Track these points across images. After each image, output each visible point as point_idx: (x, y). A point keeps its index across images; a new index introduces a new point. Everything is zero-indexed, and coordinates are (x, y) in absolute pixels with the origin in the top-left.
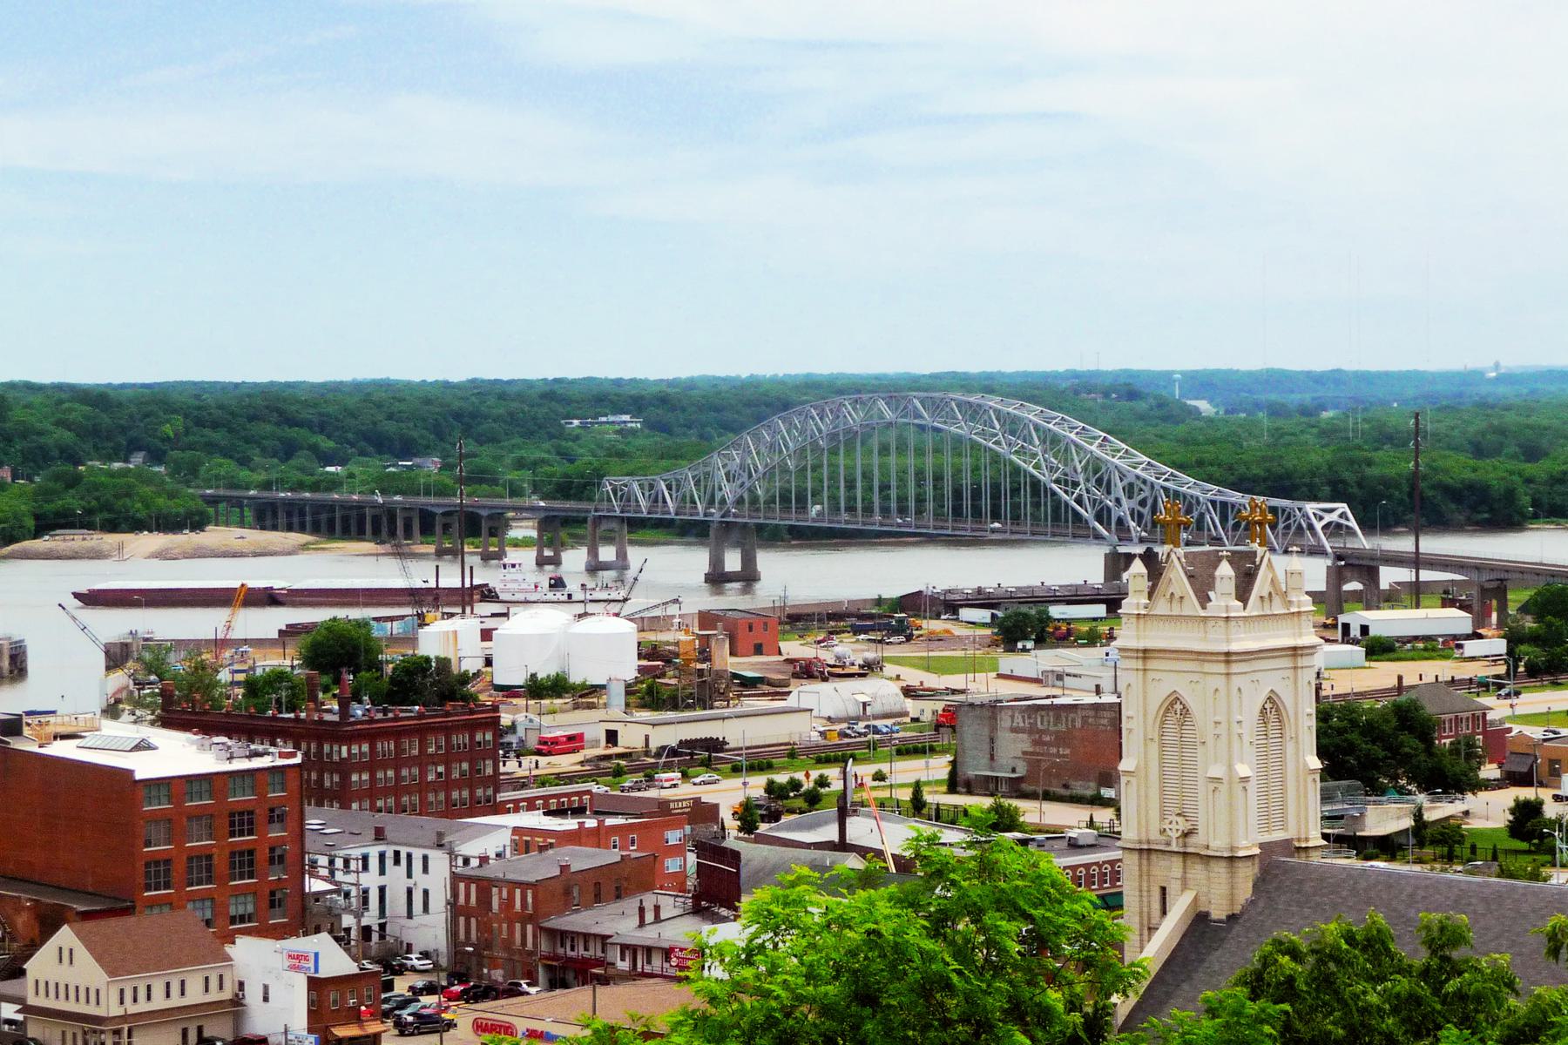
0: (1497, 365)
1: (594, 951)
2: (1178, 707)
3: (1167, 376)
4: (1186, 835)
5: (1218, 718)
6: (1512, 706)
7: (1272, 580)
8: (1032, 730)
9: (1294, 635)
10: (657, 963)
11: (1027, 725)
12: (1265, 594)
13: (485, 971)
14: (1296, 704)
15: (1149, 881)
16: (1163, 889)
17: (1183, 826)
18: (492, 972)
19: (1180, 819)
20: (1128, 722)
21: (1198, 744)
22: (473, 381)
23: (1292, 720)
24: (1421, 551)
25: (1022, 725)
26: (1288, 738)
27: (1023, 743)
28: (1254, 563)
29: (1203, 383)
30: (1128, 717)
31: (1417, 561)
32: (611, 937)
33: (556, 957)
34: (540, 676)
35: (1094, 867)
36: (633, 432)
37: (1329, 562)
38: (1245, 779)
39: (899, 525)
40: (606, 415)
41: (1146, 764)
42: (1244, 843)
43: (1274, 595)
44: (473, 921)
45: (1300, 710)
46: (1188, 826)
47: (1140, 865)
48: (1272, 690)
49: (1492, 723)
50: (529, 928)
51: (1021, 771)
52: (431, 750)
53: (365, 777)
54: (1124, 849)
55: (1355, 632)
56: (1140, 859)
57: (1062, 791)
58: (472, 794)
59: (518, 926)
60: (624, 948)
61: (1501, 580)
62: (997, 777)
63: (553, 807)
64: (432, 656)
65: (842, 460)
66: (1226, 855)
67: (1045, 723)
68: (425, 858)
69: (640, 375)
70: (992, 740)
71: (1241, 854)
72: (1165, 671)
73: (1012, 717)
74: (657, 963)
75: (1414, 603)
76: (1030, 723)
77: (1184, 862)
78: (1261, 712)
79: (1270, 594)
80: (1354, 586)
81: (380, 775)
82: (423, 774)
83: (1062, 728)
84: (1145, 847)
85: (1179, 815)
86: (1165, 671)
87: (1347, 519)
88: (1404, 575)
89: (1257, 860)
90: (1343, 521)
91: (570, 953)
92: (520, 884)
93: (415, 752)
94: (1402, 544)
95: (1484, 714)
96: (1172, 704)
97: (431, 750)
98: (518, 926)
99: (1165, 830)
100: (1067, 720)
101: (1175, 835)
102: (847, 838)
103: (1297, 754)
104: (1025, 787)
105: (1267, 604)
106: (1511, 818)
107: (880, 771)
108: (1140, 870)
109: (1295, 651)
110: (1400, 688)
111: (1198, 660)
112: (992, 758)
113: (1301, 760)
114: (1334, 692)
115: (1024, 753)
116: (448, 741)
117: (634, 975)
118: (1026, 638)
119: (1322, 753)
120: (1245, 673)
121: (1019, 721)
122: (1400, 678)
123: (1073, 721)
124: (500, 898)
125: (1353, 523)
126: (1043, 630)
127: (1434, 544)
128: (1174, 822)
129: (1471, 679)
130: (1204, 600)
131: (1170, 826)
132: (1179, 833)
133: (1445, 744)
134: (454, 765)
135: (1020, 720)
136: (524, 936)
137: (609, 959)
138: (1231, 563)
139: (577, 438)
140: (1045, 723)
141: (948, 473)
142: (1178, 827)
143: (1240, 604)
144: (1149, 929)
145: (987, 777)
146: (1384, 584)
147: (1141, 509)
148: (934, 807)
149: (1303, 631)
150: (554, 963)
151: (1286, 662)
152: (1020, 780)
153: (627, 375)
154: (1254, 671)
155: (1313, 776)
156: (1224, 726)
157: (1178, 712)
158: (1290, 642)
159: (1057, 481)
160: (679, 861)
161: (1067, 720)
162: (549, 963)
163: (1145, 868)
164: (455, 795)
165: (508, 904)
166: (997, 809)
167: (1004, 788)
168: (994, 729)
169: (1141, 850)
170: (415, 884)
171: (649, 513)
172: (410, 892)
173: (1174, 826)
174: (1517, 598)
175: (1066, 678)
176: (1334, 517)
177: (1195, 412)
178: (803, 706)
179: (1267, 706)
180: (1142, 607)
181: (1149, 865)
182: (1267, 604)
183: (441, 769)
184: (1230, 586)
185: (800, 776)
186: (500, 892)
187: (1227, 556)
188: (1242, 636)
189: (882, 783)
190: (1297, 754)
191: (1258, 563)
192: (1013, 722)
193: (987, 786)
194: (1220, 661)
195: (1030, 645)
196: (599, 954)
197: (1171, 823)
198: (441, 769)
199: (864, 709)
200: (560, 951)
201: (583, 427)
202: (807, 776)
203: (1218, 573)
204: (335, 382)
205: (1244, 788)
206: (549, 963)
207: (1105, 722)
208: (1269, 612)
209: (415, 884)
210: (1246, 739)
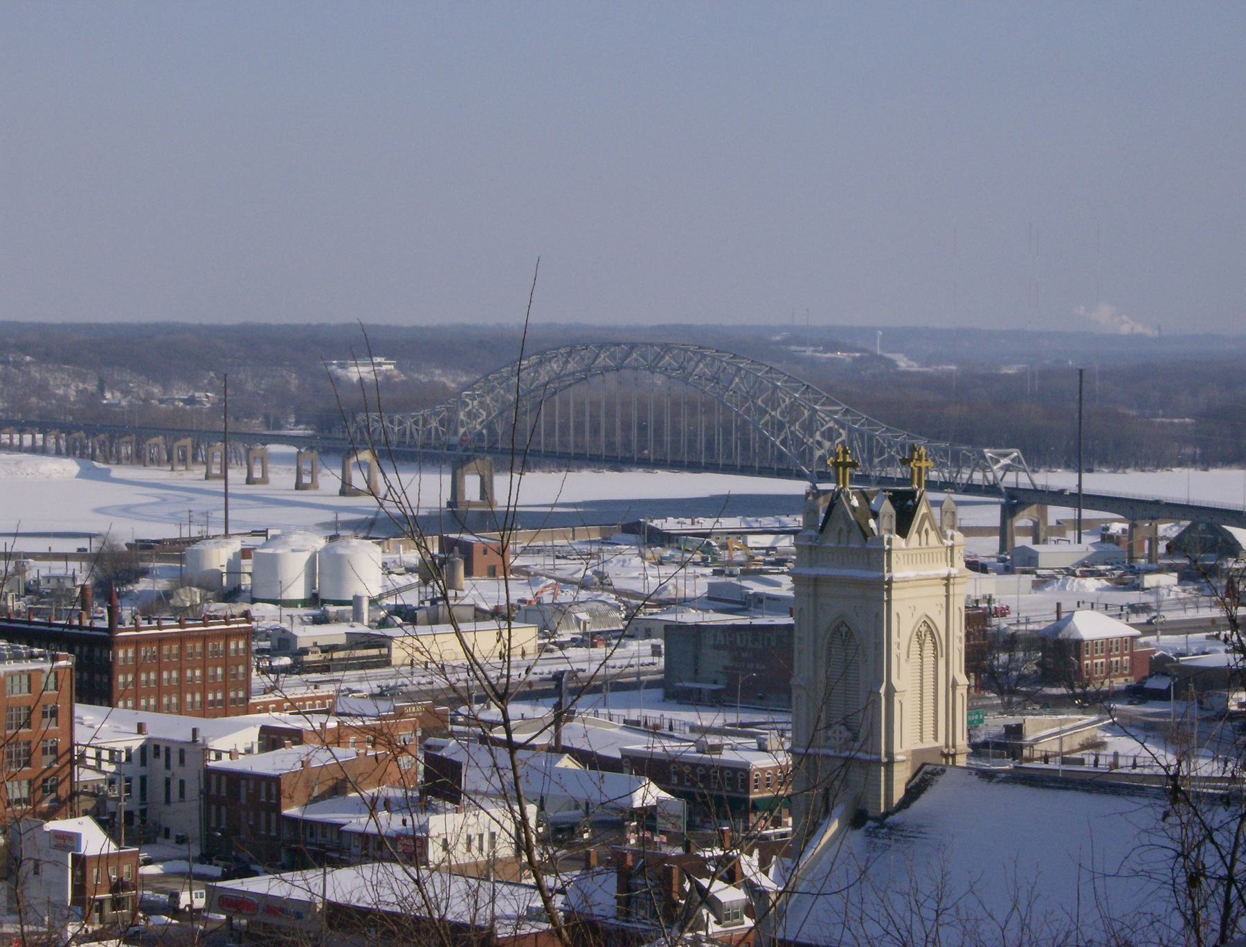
28: (913, 501)
35: (740, 773)
70: (696, 657)
73: (715, 636)
76: (731, 642)
96: (838, 628)
110: (597, 610)
112: (696, 671)
115: (726, 668)
121: (721, 639)
132: (842, 741)
133: (1096, 664)
172: (168, 782)
192: (715, 640)
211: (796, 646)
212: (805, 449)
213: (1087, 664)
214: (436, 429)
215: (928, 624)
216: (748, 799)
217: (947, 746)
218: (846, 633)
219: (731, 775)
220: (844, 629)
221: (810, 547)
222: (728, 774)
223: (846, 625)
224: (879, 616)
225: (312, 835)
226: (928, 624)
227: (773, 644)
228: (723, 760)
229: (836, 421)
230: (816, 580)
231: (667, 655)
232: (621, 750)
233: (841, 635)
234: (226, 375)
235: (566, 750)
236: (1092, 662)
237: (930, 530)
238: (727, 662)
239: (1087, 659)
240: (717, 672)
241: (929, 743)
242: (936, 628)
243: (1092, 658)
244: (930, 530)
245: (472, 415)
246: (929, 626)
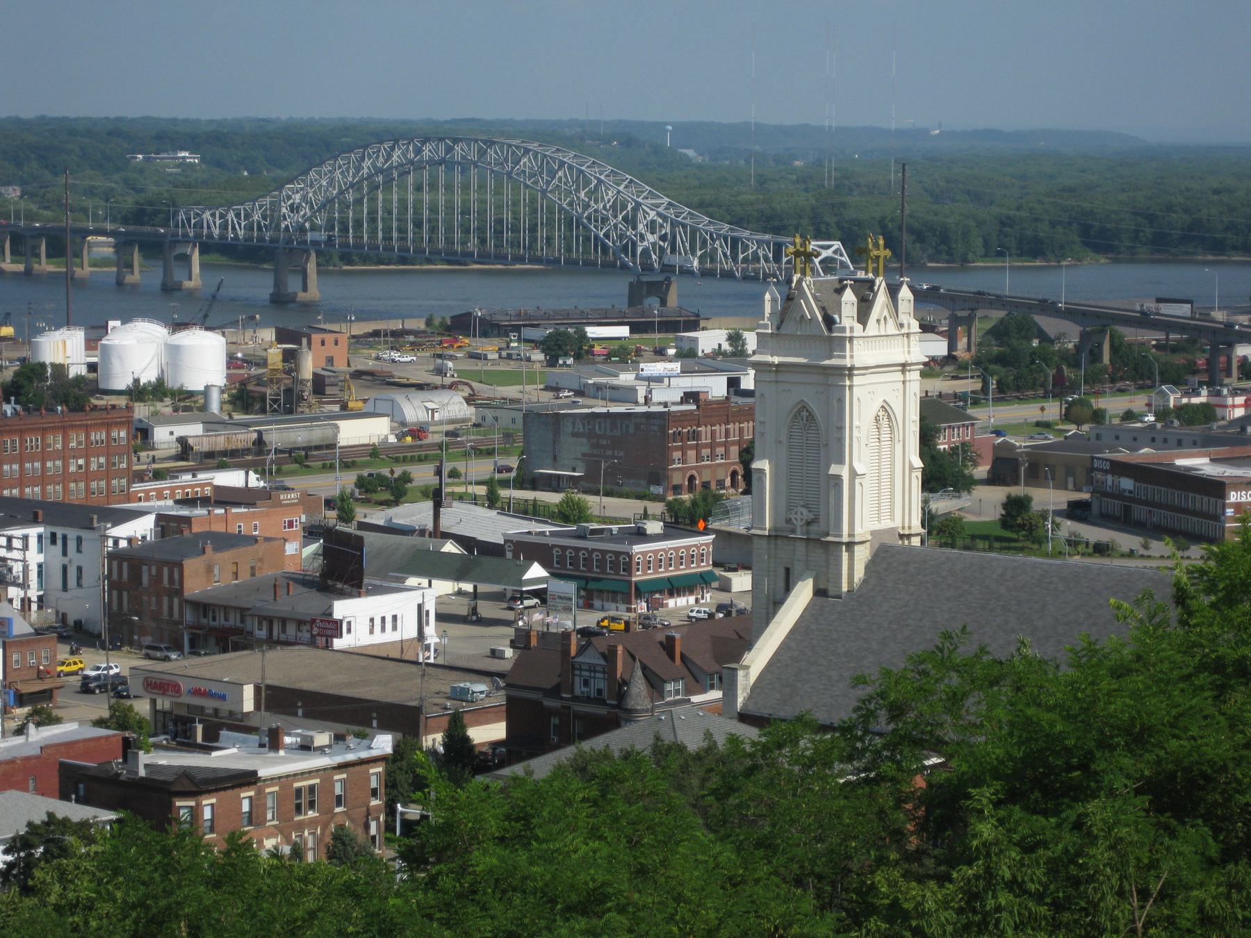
0: (940, 125)
1: (233, 621)
3: (660, 127)
8: (590, 435)
10: (291, 630)
13: (136, 637)
16: (787, 570)
18: (142, 639)
22: (43, 118)
25: (582, 430)
29: (688, 132)
32: (248, 609)
33: (199, 627)
34: (143, 381)
35: (624, 556)
36: (192, 165)
40: (167, 151)
44: (125, 594)
46: (811, 516)
50: (176, 601)
52: (73, 444)
53: (16, 467)
58: (108, 484)
59: (165, 599)
60: (262, 618)
64: (48, 362)
65: (426, 197)
68: (79, 540)
69: (193, 116)
72: (793, 383)
73: (574, 424)
74: (291, 630)
77: (807, 547)
81: (49, 464)
82: (66, 466)
83: (617, 433)
85: (803, 506)
86: (793, 383)
87: (842, 255)
91: (212, 623)
92: (166, 563)
93: (59, 446)
96: (799, 412)
97: (73, 444)
98: (165, 599)
100: (622, 427)
101: (799, 523)
106: (1003, 512)
107: (455, 469)
115: (584, 455)
116: (87, 437)
117: (272, 643)
118: (566, 355)
121: (580, 427)
124: (150, 574)
125: (846, 259)
126: (581, 348)
132: (804, 522)
134: (92, 459)
135: (581, 426)
136: (171, 608)
137: (249, 628)
139: (141, 171)
141: (474, 207)
143: (861, 326)
144: (775, 603)
147: (661, 243)
148: (532, 503)
150: (198, 632)
153: (181, 115)
157: (805, 419)
161: (622, 427)
162: (194, 631)
164: (94, 485)
165: (157, 579)
166: (568, 502)
170: (70, 561)
172: (65, 569)
176: (828, 253)
177: (687, 161)
179: (880, 414)
183: (81, 462)
186: (150, 570)
189: (456, 480)
195: (570, 361)
196: (238, 624)
198: (81, 462)
200: (204, 621)
201: (147, 160)
204: (43, 123)
206: (194, 631)
207: (656, 428)
208: (883, 333)
209: (70, 561)
210: (864, 441)
212: (627, 242)
214: (259, 223)
215: (885, 408)
216: (631, 581)
217: (903, 528)
220: (805, 414)
224: (841, 401)
225: (214, 619)
226: (885, 408)
227: (632, 431)
228: (1137, 534)
229: (659, 214)
231: (77, 448)
232: (504, 535)
234: (904, 165)
235: (447, 536)
237: (888, 317)
238: (586, 449)
241: (886, 524)
244: (888, 317)
245: (294, 209)
246: (886, 411)
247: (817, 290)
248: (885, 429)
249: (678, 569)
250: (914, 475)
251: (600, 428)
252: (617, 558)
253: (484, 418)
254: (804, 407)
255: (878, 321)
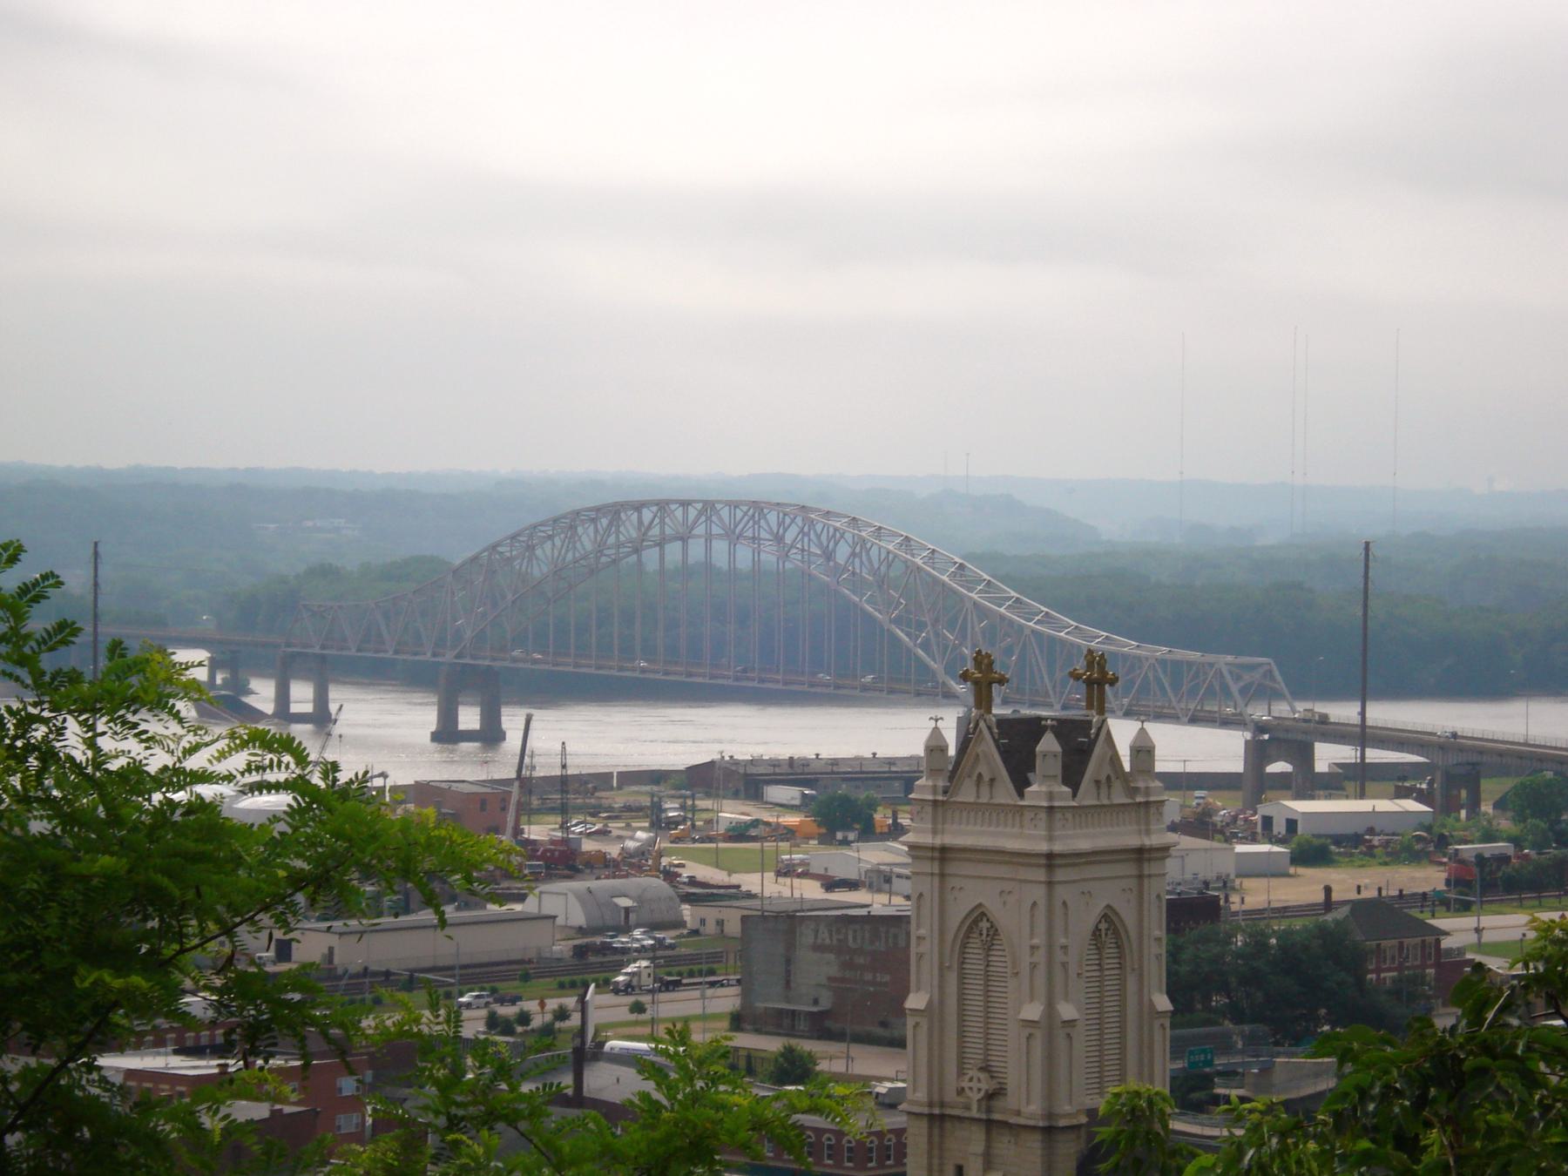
2: (984, 925)
4: (991, 1096)
5: (1036, 941)
6: (1478, 930)
7: (1111, 759)
9: (1140, 832)
11: (835, 942)
12: (1103, 778)
14: (1140, 921)
15: (941, 1157)
17: (986, 1085)
19: (982, 1076)
20: (918, 945)
21: (1009, 975)
23: (1135, 946)
24: (1369, 722)
25: (828, 941)
26: (1128, 969)
27: (828, 966)
28: (1088, 736)
30: (919, 938)
31: (1363, 736)
37: (1248, 735)
38: (1071, 1023)
39: (643, 670)
41: (942, 1002)
42: (1067, 1108)
43: (1113, 779)
45: (1146, 932)
47: (930, 1136)
48: (1108, 906)
49: (1449, 951)
51: (826, 1003)
54: (909, 1113)
55: (1279, 828)
56: (930, 1128)
57: (880, 1031)
61: (1473, 764)
62: (794, 1011)
63: (189, 1043)
66: (1041, 1124)
67: (859, 941)
70: (788, 961)
71: (1062, 1123)
75: (1358, 793)
76: (839, 940)
78: (1094, 934)
79: (1108, 778)
80: (1279, 767)
84: (936, 1111)
87: (1273, 679)
88: (1345, 753)
89: (1083, 1131)
90: (1268, 682)
94: (1344, 712)
95: (1438, 942)
96: (976, 922)
99: (963, 1089)
101: (976, 1096)
102: (585, 1090)
103: (1141, 990)
104: (829, 1024)
105: (1104, 790)
108: (930, 1142)
109: (1141, 855)
110: (1328, 904)
111: (1013, 863)
112: (788, 983)
113: (1146, 999)
114: (1245, 907)
115: (830, 979)
119: (1174, 990)
120: (1074, 882)
122: (1328, 890)
123: (896, 936)
127: (1384, 714)
128: (975, 1080)
129: (1424, 894)
130: (1021, 784)
131: (971, 1084)
132: (982, 1094)
133: (1385, 978)
135: (827, 935)
138: (1058, 735)
140: (859, 941)
142: (979, 1085)
145: (781, 1012)
146: (1321, 766)
149: (1152, 827)
151: (1128, 869)
152: (822, 1015)
154: (1084, 880)
155: (1162, 1021)
156: (1042, 952)
157: (985, 932)
158: (1133, 841)
159: (897, 621)
160: (355, 1118)
163: (936, 1139)
166: (789, 1053)
167: (802, 1025)
168: (791, 946)
169: (931, 1117)
171: (359, 650)
173: (974, 1084)
174: (1492, 789)
175: (895, 880)
178: (546, 911)
179: (1100, 926)
180: (940, 791)
181: (942, 1136)
182: (1104, 790)
184: (1056, 768)
185: (531, 1006)
187: (1053, 726)
188: (1070, 832)
190: (1141, 990)
191: (1092, 736)
192: (816, 937)
193: (781, 1022)
194: (1039, 866)
195: (851, 836)
197: (971, 1080)
199: (627, 917)
202: (542, 1005)
203: (1040, 748)
205: (1068, 1035)
208: (1106, 802)
210: (1073, 969)
211: (913, 950)
213: (1372, 979)
218: (988, 930)
219: (833, 1142)
221: (935, 802)
222: (829, 1139)
223: (988, 920)
230: (944, 854)
233: (981, 934)
236: (1378, 976)
238: (834, 971)
239: (1372, 972)
240: (819, 985)
242: (966, 918)
243: (1378, 971)
247: (1002, 734)
248: (1110, 950)
249: (884, 1167)
250: (1157, 1024)
251: (855, 938)
252: (839, 1141)
253: (703, 922)
254: (983, 914)
255: (1097, 783)
